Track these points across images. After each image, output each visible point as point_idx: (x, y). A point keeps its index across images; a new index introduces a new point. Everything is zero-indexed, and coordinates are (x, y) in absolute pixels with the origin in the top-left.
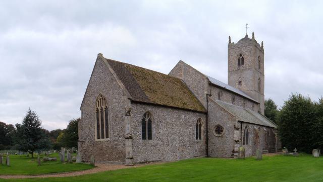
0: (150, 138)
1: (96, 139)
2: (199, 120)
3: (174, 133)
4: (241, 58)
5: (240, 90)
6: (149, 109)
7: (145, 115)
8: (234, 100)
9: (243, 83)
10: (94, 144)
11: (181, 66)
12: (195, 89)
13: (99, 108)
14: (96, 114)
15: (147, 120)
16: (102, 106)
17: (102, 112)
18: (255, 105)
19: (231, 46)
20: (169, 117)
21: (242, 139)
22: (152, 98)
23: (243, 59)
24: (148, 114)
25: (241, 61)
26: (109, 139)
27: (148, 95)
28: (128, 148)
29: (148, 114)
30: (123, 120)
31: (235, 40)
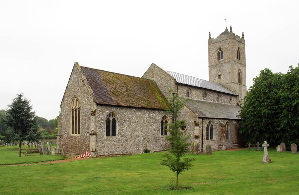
0: (114, 134)
1: (72, 135)
2: (164, 117)
3: (139, 128)
4: (220, 52)
5: (220, 84)
6: (113, 110)
7: (110, 115)
8: (205, 95)
9: (223, 77)
10: (69, 138)
11: (154, 68)
12: (163, 88)
13: (74, 107)
14: (71, 112)
15: (111, 119)
16: (76, 106)
17: (76, 111)
18: (233, 98)
19: (211, 41)
20: (134, 116)
21: (205, 133)
22: (115, 100)
23: (222, 53)
24: (112, 114)
25: (220, 55)
26: (80, 135)
27: (114, 98)
28: (93, 142)
29: (112, 114)
30: (89, 118)
31: (215, 36)
